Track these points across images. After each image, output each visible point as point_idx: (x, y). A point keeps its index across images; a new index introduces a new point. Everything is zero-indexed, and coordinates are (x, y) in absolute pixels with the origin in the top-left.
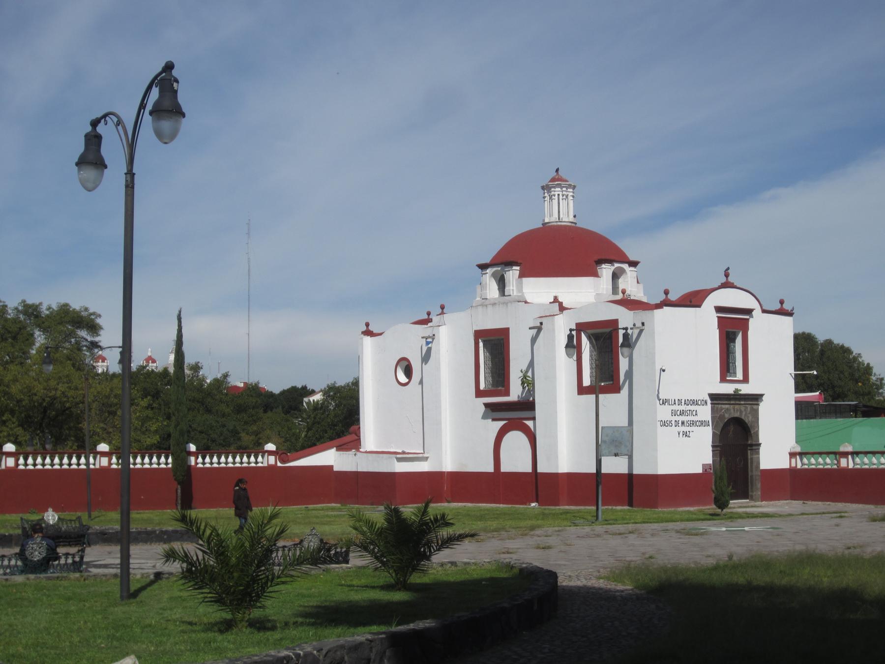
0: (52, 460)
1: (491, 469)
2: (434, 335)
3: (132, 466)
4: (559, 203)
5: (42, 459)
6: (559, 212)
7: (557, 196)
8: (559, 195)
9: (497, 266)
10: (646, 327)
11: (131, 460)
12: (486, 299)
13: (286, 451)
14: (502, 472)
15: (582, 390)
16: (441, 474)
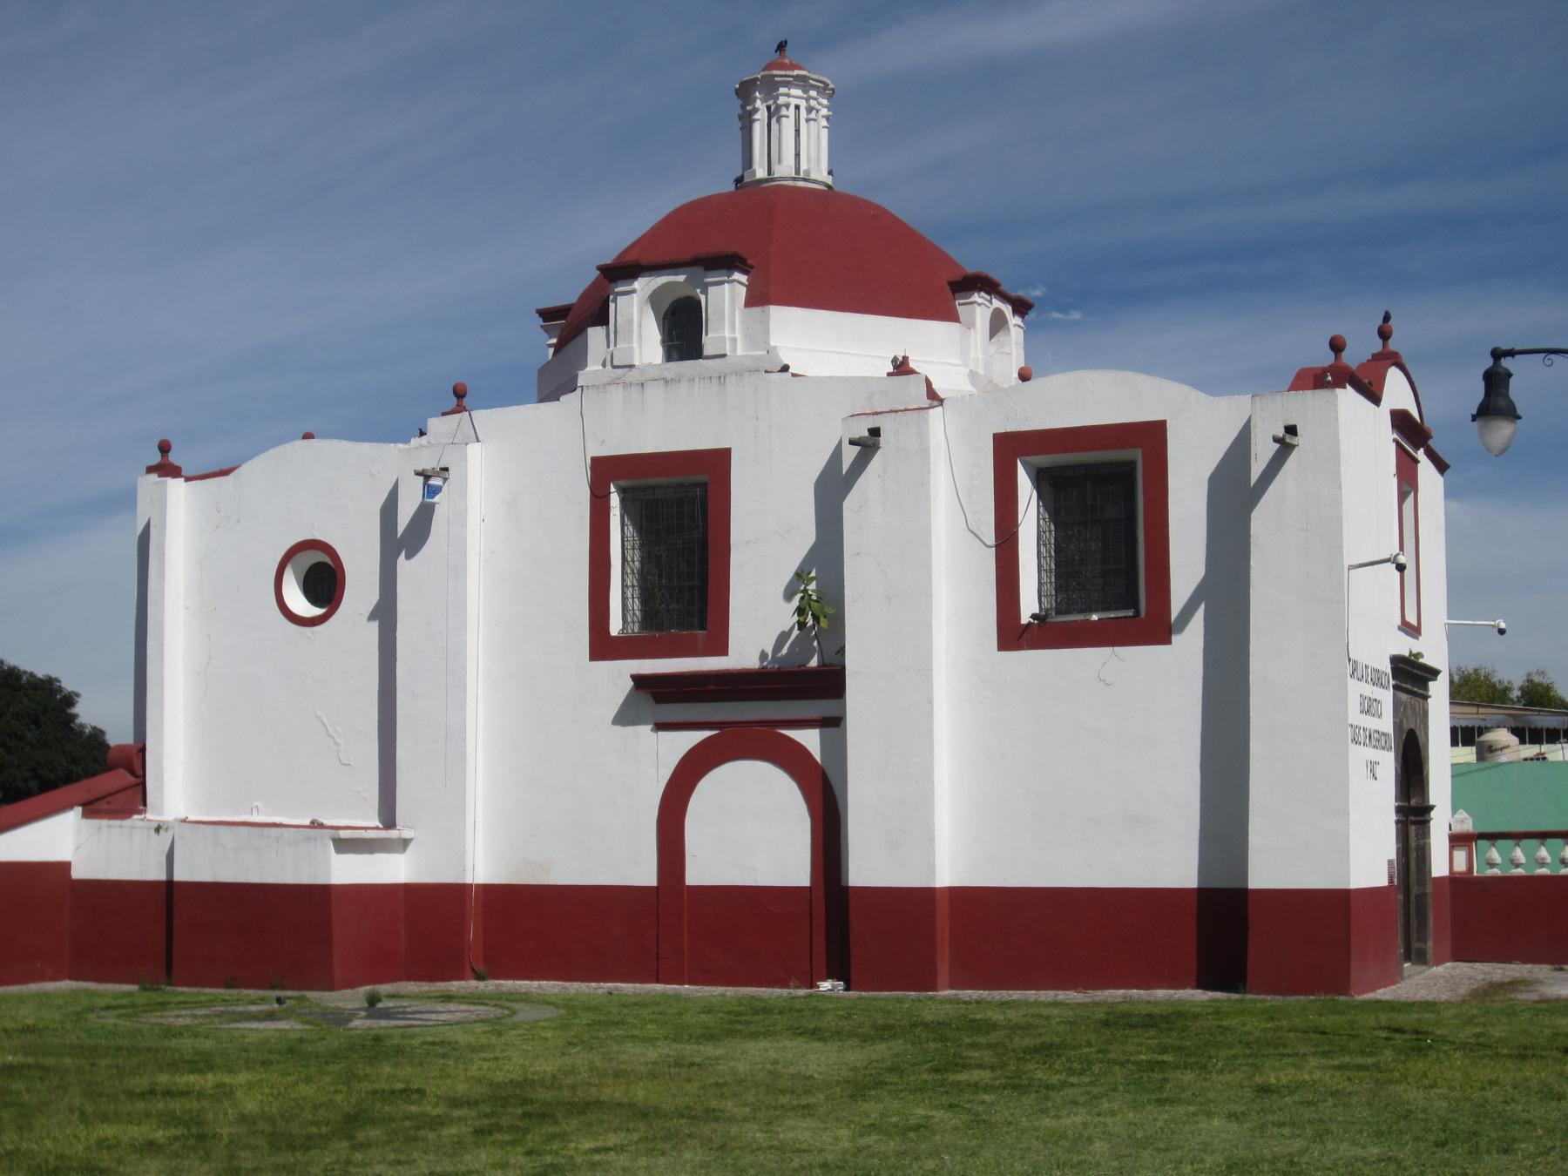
1: (644, 873)
2: (446, 469)
4: (797, 131)
6: (797, 155)
7: (792, 108)
8: (797, 107)
9: (672, 271)
12: (631, 366)
14: (689, 886)
15: (1012, 634)
16: (926, 896)
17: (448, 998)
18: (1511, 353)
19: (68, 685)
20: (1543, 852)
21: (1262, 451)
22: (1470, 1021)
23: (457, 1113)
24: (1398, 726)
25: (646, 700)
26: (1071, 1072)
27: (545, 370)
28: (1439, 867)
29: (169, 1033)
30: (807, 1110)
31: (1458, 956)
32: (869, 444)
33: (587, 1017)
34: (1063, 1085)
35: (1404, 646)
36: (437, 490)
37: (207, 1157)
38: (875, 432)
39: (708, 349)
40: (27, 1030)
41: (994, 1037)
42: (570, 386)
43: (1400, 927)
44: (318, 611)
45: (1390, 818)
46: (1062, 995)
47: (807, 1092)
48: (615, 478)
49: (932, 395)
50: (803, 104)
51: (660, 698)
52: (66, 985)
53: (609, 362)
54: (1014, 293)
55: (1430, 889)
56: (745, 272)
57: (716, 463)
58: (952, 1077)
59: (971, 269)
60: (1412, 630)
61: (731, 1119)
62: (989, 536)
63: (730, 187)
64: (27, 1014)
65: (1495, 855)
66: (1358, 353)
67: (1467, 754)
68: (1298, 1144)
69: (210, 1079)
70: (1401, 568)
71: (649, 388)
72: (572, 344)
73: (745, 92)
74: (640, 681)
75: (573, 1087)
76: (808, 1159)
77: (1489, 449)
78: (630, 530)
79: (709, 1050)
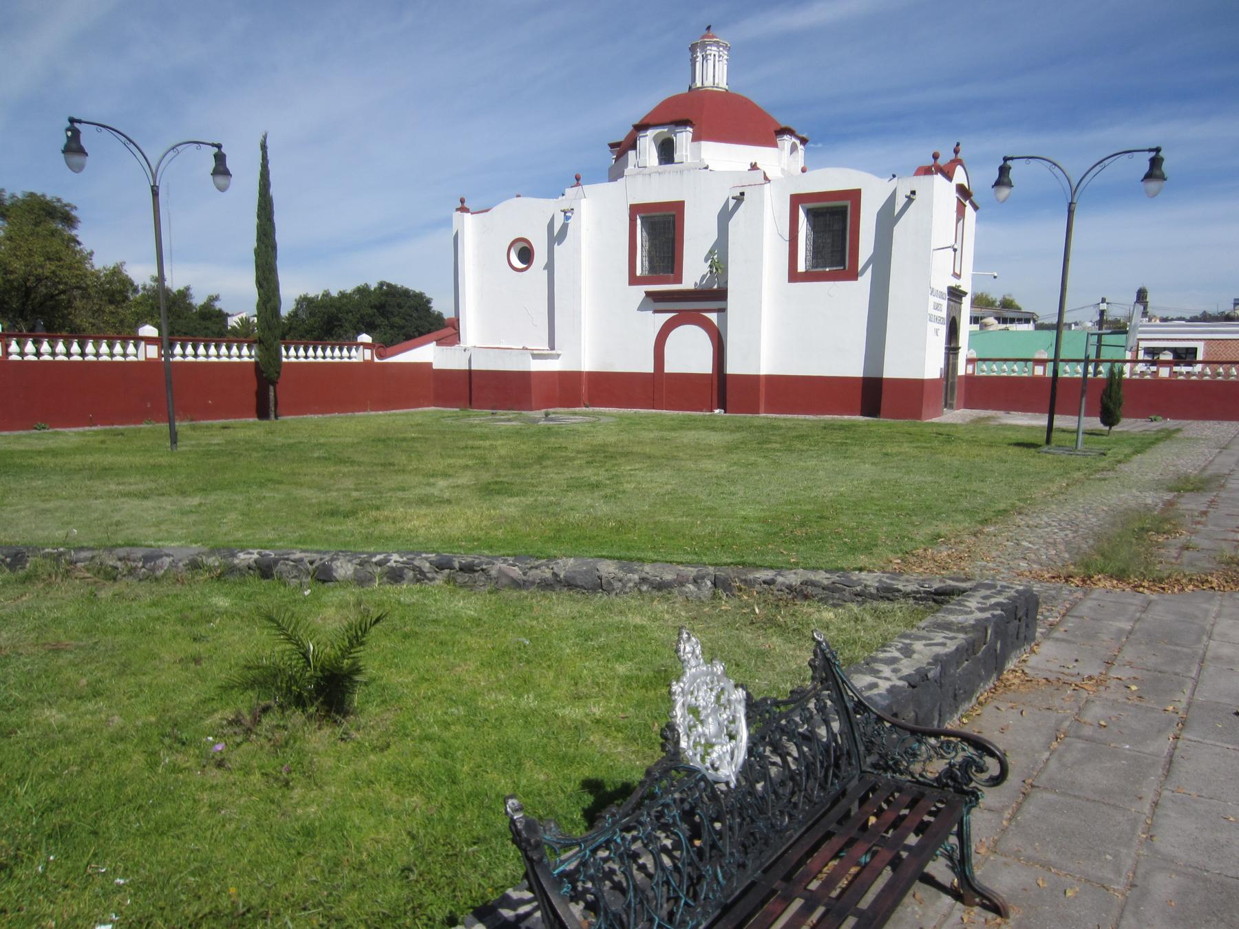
0: (68, 348)
1: (649, 368)
3: (284, 360)
5: (79, 346)
10: (917, 197)
11: (284, 353)
13: (384, 345)
15: (794, 276)
16: (577, 375)
17: (575, 414)
18: (1012, 159)
19: (428, 295)
20: (1005, 367)
21: (900, 201)
22: (970, 431)
23: (579, 456)
24: (948, 315)
25: (650, 300)
26: (811, 445)
27: (611, 170)
28: (961, 371)
29: (472, 426)
30: (710, 457)
31: (967, 406)
32: (740, 198)
33: (627, 421)
34: (807, 450)
35: (954, 282)
36: (570, 217)
37: (488, 470)
38: (742, 194)
39: (676, 161)
40: (420, 425)
41: (781, 432)
42: (621, 175)
43: (943, 394)
44: (524, 266)
45: (943, 351)
46: (807, 417)
47: (710, 450)
48: (639, 212)
49: (766, 178)
50: (717, 54)
51: (656, 300)
52: (433, 408)
53: (637, 166)
54: (801, 135)
55: (956, 380)
56: (691, 127)
57: (679, 207)
58: (765, 446)
59: (783, 125)
60: (957, 276)
61: (682, 459)
62: (787, 236)
63: (686, 90)
64: (418, 419)
65: (984, 367)
66: (946, 158)
67: (976, 327)
68: (899, 475)
69: (488, 443)
70: (955, 250)
71: (653, 175)
72: (622, 158)
73: (693, 49)
74: (648, 294)
75: (623, 447)
76: (710, 475)
77: (998, 200)
78: (644, 234)
79: (673, 434)
